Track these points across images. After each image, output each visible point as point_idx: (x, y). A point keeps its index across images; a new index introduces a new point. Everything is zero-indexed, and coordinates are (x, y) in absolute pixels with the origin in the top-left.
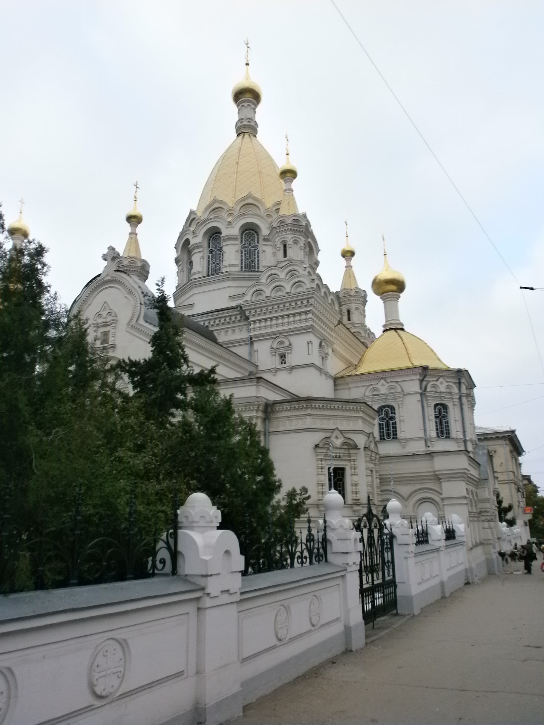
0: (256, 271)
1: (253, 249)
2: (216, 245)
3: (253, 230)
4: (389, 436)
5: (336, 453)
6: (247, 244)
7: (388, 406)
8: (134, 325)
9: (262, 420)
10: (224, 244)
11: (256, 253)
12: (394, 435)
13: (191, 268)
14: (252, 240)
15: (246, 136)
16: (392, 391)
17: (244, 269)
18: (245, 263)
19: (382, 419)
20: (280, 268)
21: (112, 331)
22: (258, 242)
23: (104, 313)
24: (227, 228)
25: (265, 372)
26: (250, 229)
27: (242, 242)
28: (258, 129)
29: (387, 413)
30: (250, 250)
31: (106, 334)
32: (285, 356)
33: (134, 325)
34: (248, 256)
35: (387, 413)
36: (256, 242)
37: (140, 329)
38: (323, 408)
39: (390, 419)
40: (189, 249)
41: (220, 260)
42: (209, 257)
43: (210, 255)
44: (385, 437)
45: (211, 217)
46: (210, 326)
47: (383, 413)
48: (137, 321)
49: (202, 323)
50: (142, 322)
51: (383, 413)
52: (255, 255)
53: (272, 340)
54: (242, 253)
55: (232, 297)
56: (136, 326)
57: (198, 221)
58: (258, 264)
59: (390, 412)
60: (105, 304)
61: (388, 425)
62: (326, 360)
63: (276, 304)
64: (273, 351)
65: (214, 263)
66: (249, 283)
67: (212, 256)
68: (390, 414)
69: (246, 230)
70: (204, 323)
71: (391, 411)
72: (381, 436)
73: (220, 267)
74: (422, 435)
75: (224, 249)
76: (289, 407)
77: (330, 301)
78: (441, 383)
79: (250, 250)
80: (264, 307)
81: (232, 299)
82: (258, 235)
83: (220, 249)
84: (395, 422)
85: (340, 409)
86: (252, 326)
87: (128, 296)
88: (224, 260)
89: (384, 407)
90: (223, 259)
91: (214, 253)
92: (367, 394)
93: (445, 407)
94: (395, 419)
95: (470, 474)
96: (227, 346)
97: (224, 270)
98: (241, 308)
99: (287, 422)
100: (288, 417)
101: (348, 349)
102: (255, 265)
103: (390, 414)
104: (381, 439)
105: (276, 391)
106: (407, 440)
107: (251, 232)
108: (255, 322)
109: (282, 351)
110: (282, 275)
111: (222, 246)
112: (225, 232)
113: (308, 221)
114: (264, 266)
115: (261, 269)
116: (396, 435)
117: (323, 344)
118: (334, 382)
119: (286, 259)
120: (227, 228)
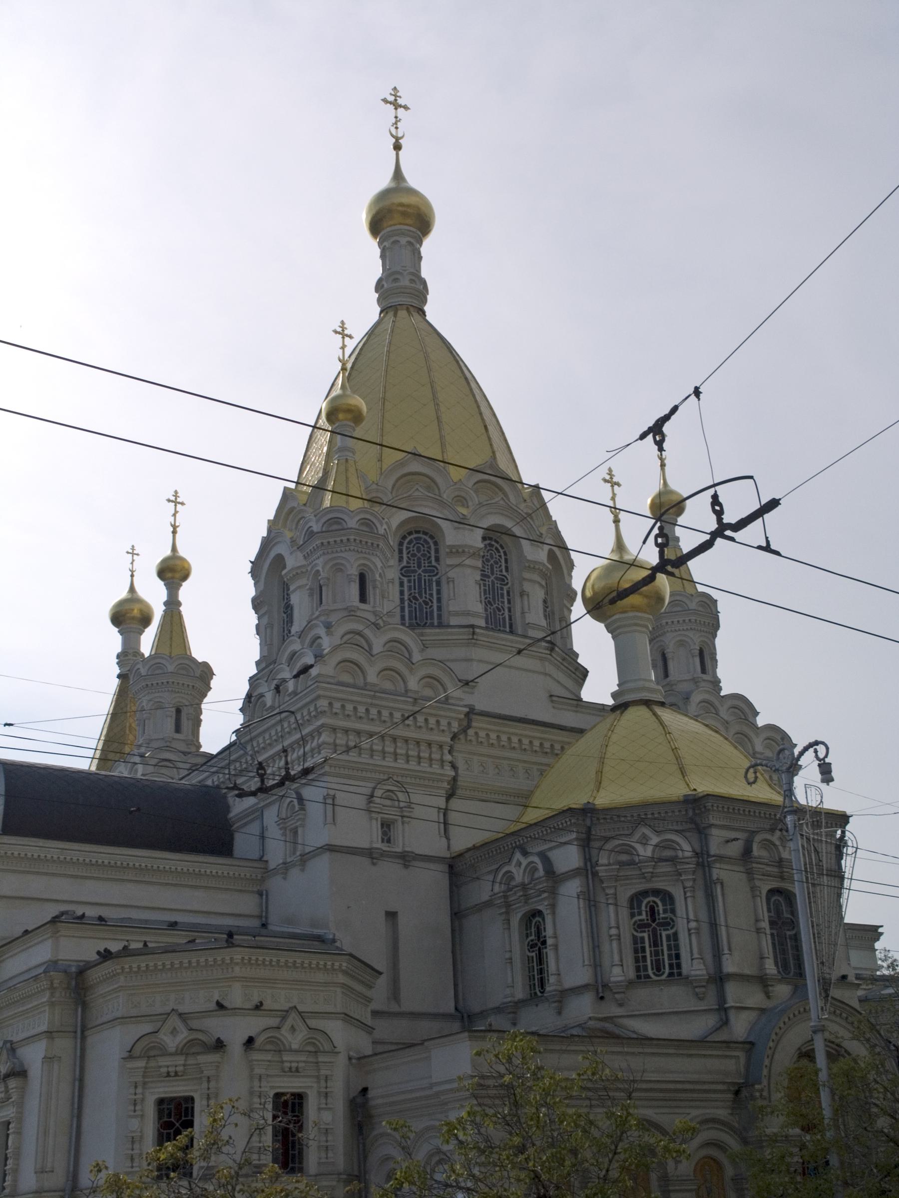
0: (436, 624)
3: (425, 533)
4: (658, 969)
6: (414, 565)
7: (656, 892)
12: (671, 966)
15: (402, 313)
16: (668, 853)
19: (640, 926)
22: (437, 559)
26: (417, 532)
27: (401, 559)
28: (428, 297)
29: (652, 911)
35: (652, 911)
36: (433, 559)
40: (281, 577)
44: (650, 972)
47: (643, 908)
51: (533, 930)
54: (402, 584)
59: (661, 908)
63: (435, 715)
69: (410, 533)
72: (638, 969)
82: (436, 543)
84: (675, 934)
85: (282, 966)
89: (645, 893)
93: (668, 898)
94: (673, 926)
96: (408, 780)
102: (432, 612)
103: (640, 917)
104: (639, 977)
107: (420, 538)
112: (451, 536)
113: (380, 314)
116: (679, 966)
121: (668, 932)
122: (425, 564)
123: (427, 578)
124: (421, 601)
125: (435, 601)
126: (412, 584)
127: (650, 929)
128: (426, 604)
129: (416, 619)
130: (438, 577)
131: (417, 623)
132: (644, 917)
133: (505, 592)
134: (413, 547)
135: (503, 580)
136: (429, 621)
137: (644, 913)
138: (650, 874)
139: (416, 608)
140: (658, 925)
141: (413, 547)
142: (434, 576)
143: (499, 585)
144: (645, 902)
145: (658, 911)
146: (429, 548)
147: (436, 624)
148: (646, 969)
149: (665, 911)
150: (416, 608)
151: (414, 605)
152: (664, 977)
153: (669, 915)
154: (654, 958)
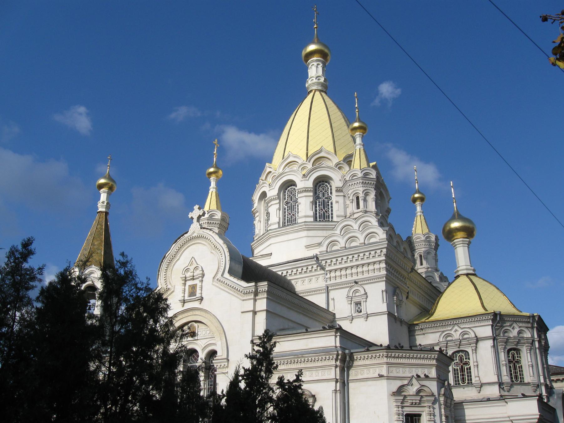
0: (330, 221)
1: (326, 200)
2: (292, 197)
4: (463, 381)
5: (416, 400)
8: (219, 279)
9: (342, 369)
10: (299, 195)
11: (330, 204)
12: (468, 380)
13: (268, 219)
14: (326, 191)
16: (466, 336)
17: (318, 219)
18: (319, 213)
20: (353, 219)
21: (199, 284)
22: (331, 193)
23: (192, 268)
24: (301, 181)
25: (342, 320)
29: (461, 360)
30: (324, 201)
31: (193, 287)
32: (360, 304)
33: (219, 279)
34: (322, 207)
36: (329, 193)
37: (225, 283)
38: (398, 357)
39: (464, 364)
41: (295, 211)
42: (285, 209)
43: (286, 207)
45: (287, 170)
46: (288, 275)
48: (222, 275)
49: (280, 273)
50: (227, 275)
52: (328, 205)
53: (348, 289)
55: (308, 247)
56: (221, 280)
57: (274, 174)
58: (332, 214)
59: (516, 355)
60: (193, 259)
61: (462, 370)
62: (400, 307)
64: (350, 299)
65: (290, 214)
66: (325, 233)
67: (288, 207)
68: (516, 357)
70: (282, 273)
71: (466, 356)
73: (296, 218)
74: (495, 379)
75: (299, 200)
76: (366, 356)
77: (402, 250)
78: (456, 331)
79: (324, 201)
80: (282, 227)
81: (307, 248)
83: (296, 202)
84: (470, 368)
86: (328, 276)
87: (213, 251)
88: (299, 211)
89: (458, 352)
90: (298, 210)
91: (289, 205)
92: (441, 340)
93: (466, 353)
94: (469, 364)
95: (544, 419)
96: (303, 295)
97: (300, 221)
98: (317, 258)
99: (365, 370)
100: (366, 365)
101: (430, 301)
102: (329, 216)
103: (516, 357)
104: (456, 384)
105: (352, 340)
106: (482, 385)
108: (330, 271)
109: (356, 300)
110: (356, 226)
111: (297, 197)
114: (338, 216)
115: (335, 219)
116: (471, 380)
117: (397, 291)
118: (409, 328)
119: (359, 210)
120: (301, 181)
121: (467, 367)
122: (326, 196)
123: (327, 201)
124: (324, 211)
125: (318, 210)
126: (289, 208)
127: (460, 366)
128: (322, 209)
129: (322, 219)
130: (331, 200)
131: (322, 220)
132: (465, 360)
133: (330, 204)
134: (321, 188)
135: (329, 198)
136: (327, 219)
137: (510, 357)
138: (459, 345)
139: (322, 214)
140: (460, 364)
141: (321, 188)
142: (330, 200)
143: (289, 205)
144: (458, 355)
145: (463, 358)
146: (328, 188)
147: (330, 221)
148: (458, 381)
149: (466, 359)
150: (322, 214)
151: (321, 213)
152: (465, 384)
153: (467, 360)
154: (462, 377)
